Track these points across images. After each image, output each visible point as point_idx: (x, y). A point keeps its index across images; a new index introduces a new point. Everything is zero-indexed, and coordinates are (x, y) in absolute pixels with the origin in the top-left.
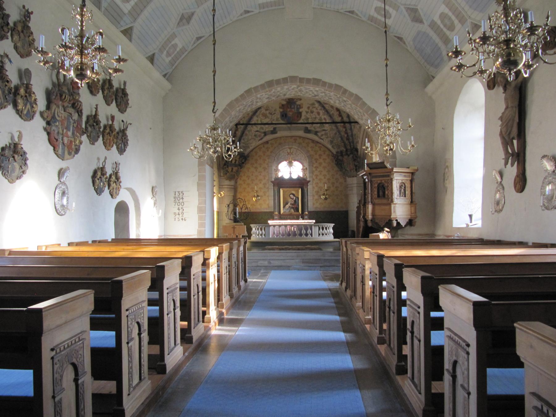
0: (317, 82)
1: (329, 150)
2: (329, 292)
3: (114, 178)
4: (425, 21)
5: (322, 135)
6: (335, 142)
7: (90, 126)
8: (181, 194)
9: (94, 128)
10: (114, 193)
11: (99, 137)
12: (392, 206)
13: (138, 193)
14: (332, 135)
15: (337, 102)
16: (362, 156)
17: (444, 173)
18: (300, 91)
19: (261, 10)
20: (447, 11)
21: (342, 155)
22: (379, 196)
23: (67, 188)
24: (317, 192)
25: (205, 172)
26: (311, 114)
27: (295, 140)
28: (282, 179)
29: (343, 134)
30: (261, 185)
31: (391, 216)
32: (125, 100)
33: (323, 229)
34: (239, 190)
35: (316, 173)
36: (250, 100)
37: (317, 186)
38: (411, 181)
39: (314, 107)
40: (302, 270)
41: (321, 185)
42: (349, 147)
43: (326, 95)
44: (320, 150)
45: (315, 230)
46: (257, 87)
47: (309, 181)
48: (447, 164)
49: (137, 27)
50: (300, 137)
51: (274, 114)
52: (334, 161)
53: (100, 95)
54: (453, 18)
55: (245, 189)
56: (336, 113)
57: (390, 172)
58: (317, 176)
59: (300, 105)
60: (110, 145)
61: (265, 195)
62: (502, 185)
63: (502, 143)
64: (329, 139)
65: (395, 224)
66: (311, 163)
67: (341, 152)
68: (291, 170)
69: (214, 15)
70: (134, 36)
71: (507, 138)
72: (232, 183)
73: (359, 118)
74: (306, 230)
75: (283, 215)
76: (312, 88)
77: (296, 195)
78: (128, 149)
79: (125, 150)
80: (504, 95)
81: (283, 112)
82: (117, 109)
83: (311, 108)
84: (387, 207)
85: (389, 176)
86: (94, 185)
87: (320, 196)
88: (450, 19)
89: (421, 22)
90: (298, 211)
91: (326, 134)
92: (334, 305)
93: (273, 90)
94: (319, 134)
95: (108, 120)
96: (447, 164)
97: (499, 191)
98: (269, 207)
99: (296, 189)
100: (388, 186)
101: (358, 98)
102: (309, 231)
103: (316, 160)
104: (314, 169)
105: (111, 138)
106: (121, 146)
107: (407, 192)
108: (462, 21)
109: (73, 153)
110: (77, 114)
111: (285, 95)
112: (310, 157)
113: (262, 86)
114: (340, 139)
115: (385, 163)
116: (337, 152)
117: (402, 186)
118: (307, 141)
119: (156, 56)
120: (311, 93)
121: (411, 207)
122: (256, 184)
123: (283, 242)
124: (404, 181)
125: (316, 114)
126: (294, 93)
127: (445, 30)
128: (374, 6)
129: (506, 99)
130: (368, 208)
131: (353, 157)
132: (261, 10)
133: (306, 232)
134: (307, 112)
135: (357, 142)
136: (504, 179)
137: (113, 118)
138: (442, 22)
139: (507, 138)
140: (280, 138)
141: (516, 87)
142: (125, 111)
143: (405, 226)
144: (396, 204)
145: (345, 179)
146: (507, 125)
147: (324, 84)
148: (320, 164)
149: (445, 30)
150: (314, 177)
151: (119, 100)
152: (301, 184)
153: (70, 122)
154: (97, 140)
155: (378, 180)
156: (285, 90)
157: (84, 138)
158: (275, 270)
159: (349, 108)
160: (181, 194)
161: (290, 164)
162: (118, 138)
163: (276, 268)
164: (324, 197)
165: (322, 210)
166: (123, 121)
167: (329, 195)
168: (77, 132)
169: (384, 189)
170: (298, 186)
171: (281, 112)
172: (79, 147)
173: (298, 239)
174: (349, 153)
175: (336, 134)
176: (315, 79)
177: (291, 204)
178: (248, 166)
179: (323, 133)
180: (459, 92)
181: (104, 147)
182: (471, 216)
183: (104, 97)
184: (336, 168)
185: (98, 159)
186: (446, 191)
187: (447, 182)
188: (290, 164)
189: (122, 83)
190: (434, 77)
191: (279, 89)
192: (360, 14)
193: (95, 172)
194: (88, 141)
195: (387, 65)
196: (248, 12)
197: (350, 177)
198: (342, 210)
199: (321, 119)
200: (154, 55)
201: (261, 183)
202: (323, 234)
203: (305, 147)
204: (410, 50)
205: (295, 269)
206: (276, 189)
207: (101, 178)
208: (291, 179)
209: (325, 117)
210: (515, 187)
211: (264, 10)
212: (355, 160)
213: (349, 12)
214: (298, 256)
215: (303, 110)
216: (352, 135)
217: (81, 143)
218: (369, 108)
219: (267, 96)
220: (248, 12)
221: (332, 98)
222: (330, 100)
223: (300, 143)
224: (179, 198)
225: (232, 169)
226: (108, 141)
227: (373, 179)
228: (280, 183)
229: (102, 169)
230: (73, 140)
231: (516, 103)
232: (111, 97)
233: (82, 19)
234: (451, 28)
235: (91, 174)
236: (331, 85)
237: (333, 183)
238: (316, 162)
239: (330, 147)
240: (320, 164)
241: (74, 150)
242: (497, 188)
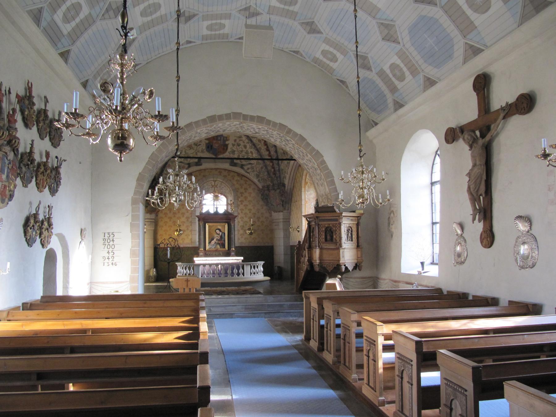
0: (261, 120)
1: (255, 184)
2: (296, 351)
3: (46, 224)
4: (373, 69)
5: (248, 169)
6: (261, 176)
7: (24, 165)
8: (112, 236)
9: (29, 168)
10: (46, 242)
11: (32, 178)
12: (341, 251)
13: (68, 238)
14: (258, 169)
15: (279, 140)
16: (289, 191)
17: (389, 218)
18: (242, 127)
19: (204, 42)
20: (399, 62)
21: (269, 190)
22: (326, 240)
26: (238, 147)
27: (220, 173)
28: (208, 213)
29: (269, 168)
30: (183, 219)
31: (339, 261)
32: (59, 133)
33: (254, 268)
34: (161, 223)
35: (241, 207)
36: (190, 135)
37: (242, 221)
38: (358, 225)
39: (241, 140)
40: (248, 317)
41: (246, 219)
42: (275, 182)
43: (268, 133)
44: (246, 183)
45: (247, 269)
46: (198, 121)
47: (236, 216)
48: (392, 209)
49: (74, 50)
50: (225, 170)
51: (200, 145)
52: (260, 195)
53: (35, 128)
54: (405, 69)
55: (166, 222)
56: (263, 148)
57: (339, 216)
58: (242, 210)
59: (226, 137)
60: (43, 186)
61: (188, 229)
62: (464, 238)
63: (470, 199)
64: (255, 173)
65: (343, 270)
66: (237, 198)
67: (268, 187)
68: (214, 203)
70: (70, 61)
71: (475, 195)
73: (299, 158)
74: (238, 270)
75: (209, 251)
76: (254, 126)
78: (61, 189)
79: (57, 191)
80: (470, 152)
81: (209, 143)
82: (50, 144)
83: (238, 141)
84: (336, 251)
85: (337, 220)
86: (25, 235)
87: (245, 231)
88: (401, 70)
89: (369, 69)
90: (224, 247)
91: (252, 168)
92: (313, 371)
93: (215, 126)
94: (246, 168)
95: (41, 157)
96: (392, 209)
97: (461, 244)
98: (192, 242)
99: (223, 224)
100: (336, 230)
101: (302, 139)
102: (241, 270)
104: (239, 203)
105: (45, 178)
106: (54, 187)
108: (414, 72)
109: (7, 200)
110: (12, 153)
111: (224, 131)
112: (235, 191)
113: (204, 121)
114: (266, 173)
115: (335, 208)
116: (263, 187)
117: (350, 230)
118: (232, 174)
119: (90, 83)
120: (252, 130)
121: (357, 251)
122: (179, 218)
123: (214, 283)
124: (351, 225)
125: (243, 147)
126: (233, 129)
127: (394, 79)
128: (322, 49)
129: (473, 157)
130: (315, 252)
131: (280, 192)
132: (204, 42)
133: (238, 271)
134: (233, 145)
135: (285, 177)
136: (464, 231)
137: (48, 154)
138: (391, 72)
139: (475, 195)
140: (205, 170)
142: (59, 145)
143: (352, 270)
144: (345, 249)
145: (270, 213)
147: (269, 122)
149: (394, 79)
152: (227, 218)
153: (5, 163)
154: (31, 181)
155: (326, 224)
156: (226, 126)
157: (18, 181)
159: (290, 147)
160: (112, 236)
161: (216, 198)
162: (48, 176)
163: (218, 316)
164: (249, 232)
165: (247, 245)
166: (57, 157)
167: (255, 231)
168: (12, 175)
169: (332, 233)
170: (225, 221)
171: (207, 144)
172: (14, 191)
173: (229, 279)
174: (276, 188)
175: (262, 168)
176: (258, 117)
177: (217, 240)
179: (249, 166)
181: (37, 189)
182: (422, 264)
183: (38, 129)
184: (261, 203)
185: (31, 203)
186: (392, 236)
187: (393, 227)
188: (216, 198)
190: (376, 124)
191: (220, 125)
192: (303, 54)
193: (27, 220)
194: (21, 183)
195: (359, 115)
196: (190, 42)
197: (275, 211)
198: (266, 245)
199: (247, 153)
200: (87, 81)
201: (183, 216)
202: (254, 273)
203: (230, 180)
204: (352, 94)
205: (239, 317)
206: (202, 224)
207: (33, 226)
208: (216, 213)
209: (252, 150)
210: (482, 242)
211: (206, 42)
212: (282, 195)
213: (294, 52)
214: (239, 302)
215: (230, 143)
216: (279, 170)
217: (15, 186)
218: (313, 149)
219: (206, 131)
220: (190, 42)
221: (274, 136)
222: (271, 139)
223: (225, 176)
224: (109, 239)
226: (42, 181)
227: (320, 223)
228: (206, 218)
229: (36, 216)
230: (7, 184)
231: (484, 161)
232: (45, 129)
233: (122, 70)
234: (402, 78)
235: (22, 222)
236: (275, 124)
237: (258, 218)
239: (256, 180)
241: (8, 196)
242: (457, 240)
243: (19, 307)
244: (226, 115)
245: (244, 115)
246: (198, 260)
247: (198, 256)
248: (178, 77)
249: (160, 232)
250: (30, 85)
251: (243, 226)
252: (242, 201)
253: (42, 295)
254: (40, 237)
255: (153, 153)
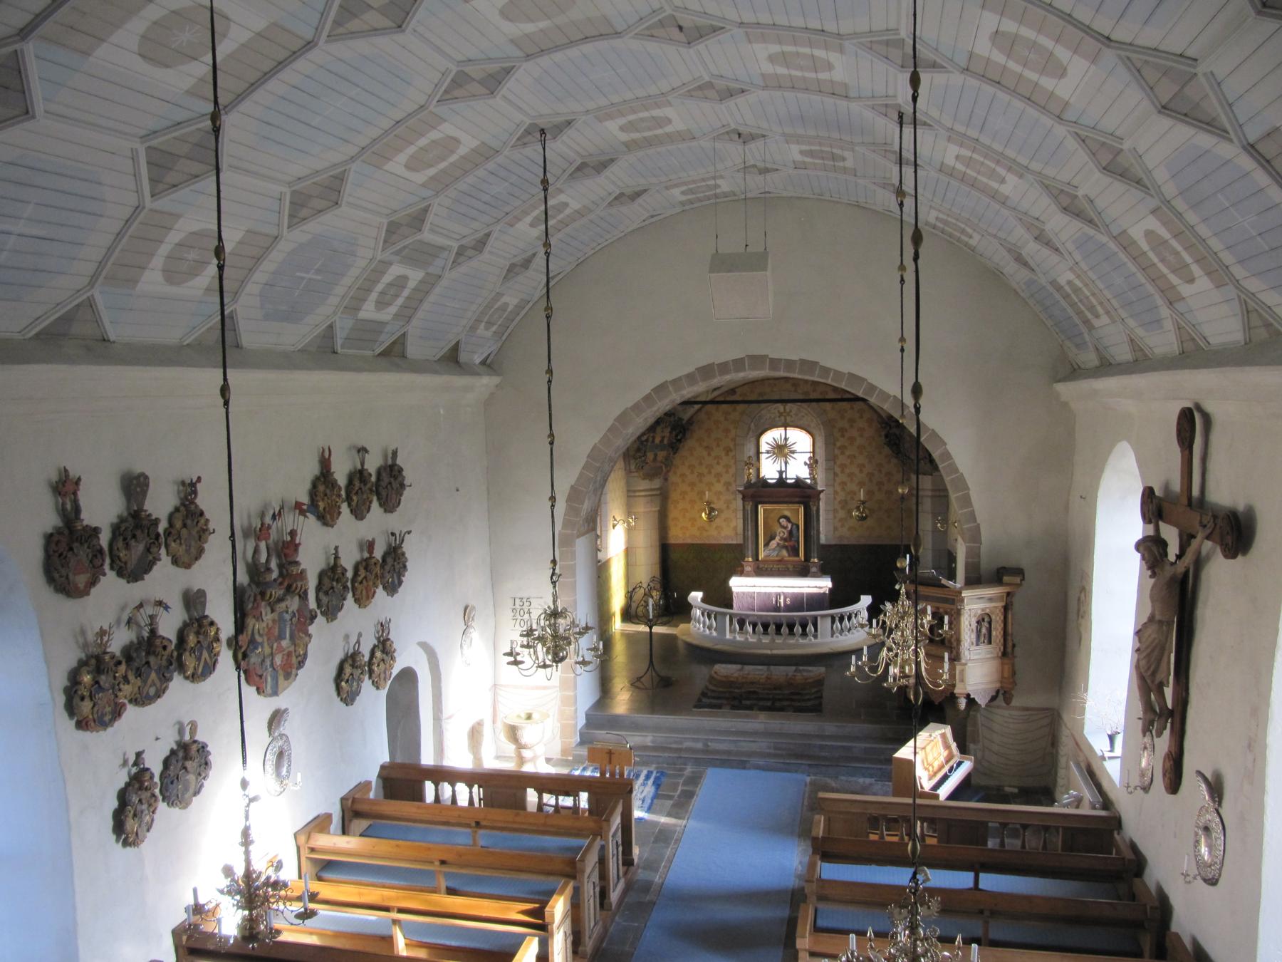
23: (289, 745)
24: (844, 504)
25: (574, 558)
28: (764, 483)
34: (674, 495)
35: (842, 459)
38: (1006, 609)
41: (852, 486)
46: (679, 379)
55: (684, 493)
58: (843, 466)
69: (550, 381)
72: (657, 483)
75: (764, 561)
77: (793, 520)
80: (1153, 581)
86: (339, 694)
87: (850, 512)
99: (795, 506)
102: (810, 628)
103: (842, 430)
104: (837, 452)
107: (994, 633)
117: (984, 620)
121: (1002, 664)
141: (1173, 579)
146: (1148, 655)
148: (852, 439)
150: (837, 470)
151: (384, 493)
152: (800, 493)
158: (715, 766)
165: (853, 542)
177: (782, 539)
178: (690, 443)
180: (1110, 452)
184: (887, 450)
185: (347, 637)
189: (390, 455)
200: (458, 343)
225: (656, 455)
228: (759, 492)
237: (880, 484)
238: (843, 436)
240: (852, 439)
243: (328, 817)
244: (736, 362)
245: (772, 360)
246: (739, 584)
247: (742, 573)
248: (551, 435)
249: (673, 513)
250: (327, 455)
251: (846, 502)
252: (843, 448)
253: (386, 758)
254: (370, 677)
255: (595, 447)
